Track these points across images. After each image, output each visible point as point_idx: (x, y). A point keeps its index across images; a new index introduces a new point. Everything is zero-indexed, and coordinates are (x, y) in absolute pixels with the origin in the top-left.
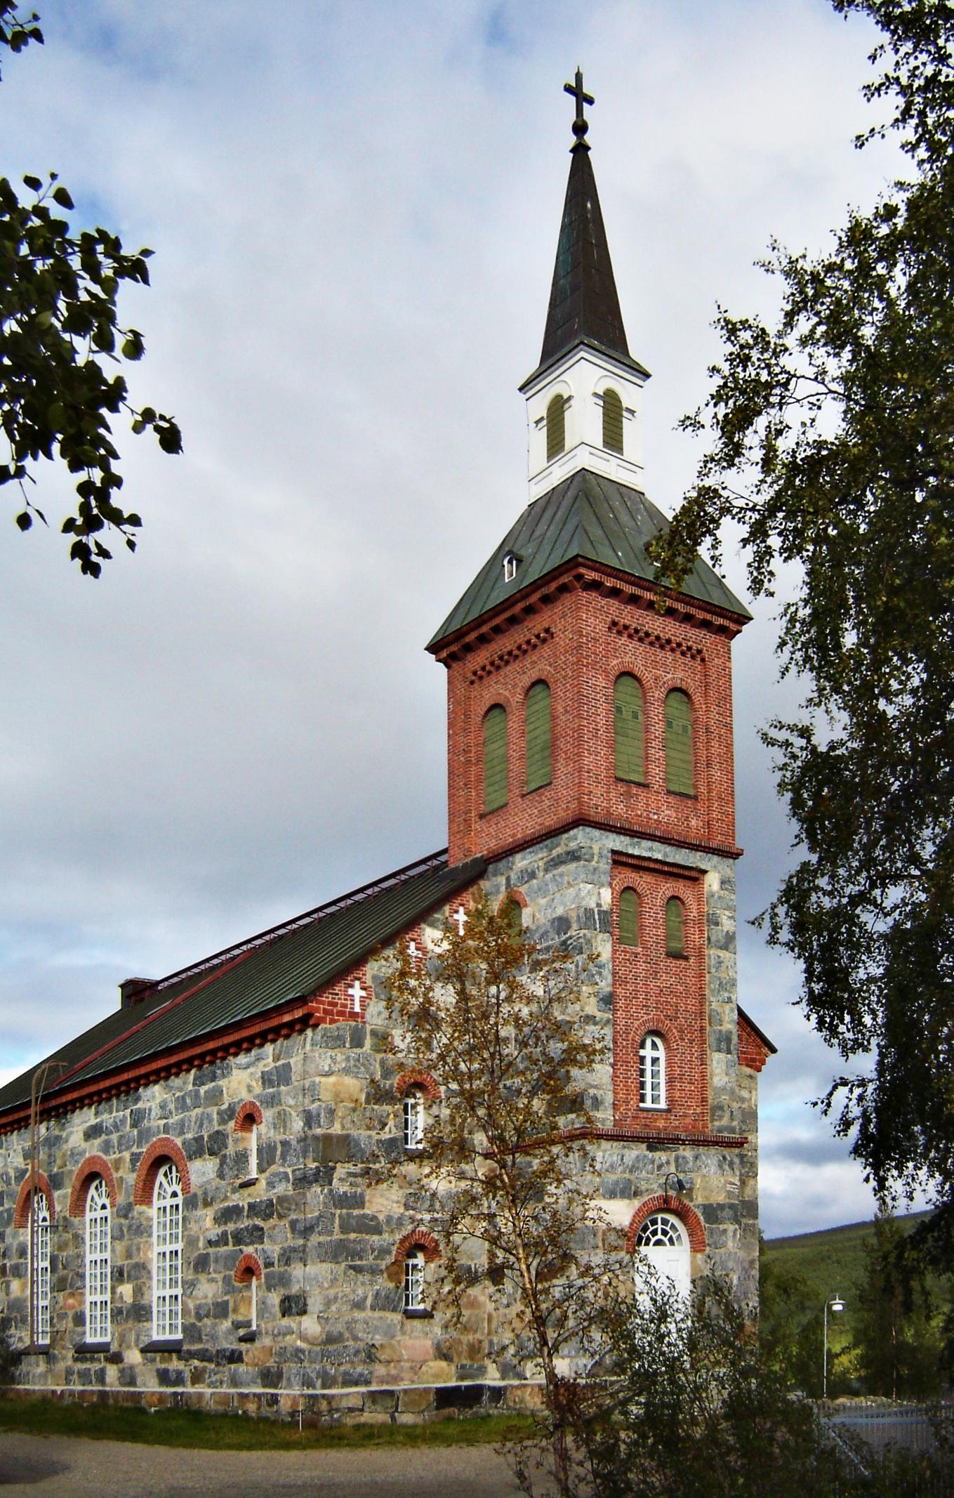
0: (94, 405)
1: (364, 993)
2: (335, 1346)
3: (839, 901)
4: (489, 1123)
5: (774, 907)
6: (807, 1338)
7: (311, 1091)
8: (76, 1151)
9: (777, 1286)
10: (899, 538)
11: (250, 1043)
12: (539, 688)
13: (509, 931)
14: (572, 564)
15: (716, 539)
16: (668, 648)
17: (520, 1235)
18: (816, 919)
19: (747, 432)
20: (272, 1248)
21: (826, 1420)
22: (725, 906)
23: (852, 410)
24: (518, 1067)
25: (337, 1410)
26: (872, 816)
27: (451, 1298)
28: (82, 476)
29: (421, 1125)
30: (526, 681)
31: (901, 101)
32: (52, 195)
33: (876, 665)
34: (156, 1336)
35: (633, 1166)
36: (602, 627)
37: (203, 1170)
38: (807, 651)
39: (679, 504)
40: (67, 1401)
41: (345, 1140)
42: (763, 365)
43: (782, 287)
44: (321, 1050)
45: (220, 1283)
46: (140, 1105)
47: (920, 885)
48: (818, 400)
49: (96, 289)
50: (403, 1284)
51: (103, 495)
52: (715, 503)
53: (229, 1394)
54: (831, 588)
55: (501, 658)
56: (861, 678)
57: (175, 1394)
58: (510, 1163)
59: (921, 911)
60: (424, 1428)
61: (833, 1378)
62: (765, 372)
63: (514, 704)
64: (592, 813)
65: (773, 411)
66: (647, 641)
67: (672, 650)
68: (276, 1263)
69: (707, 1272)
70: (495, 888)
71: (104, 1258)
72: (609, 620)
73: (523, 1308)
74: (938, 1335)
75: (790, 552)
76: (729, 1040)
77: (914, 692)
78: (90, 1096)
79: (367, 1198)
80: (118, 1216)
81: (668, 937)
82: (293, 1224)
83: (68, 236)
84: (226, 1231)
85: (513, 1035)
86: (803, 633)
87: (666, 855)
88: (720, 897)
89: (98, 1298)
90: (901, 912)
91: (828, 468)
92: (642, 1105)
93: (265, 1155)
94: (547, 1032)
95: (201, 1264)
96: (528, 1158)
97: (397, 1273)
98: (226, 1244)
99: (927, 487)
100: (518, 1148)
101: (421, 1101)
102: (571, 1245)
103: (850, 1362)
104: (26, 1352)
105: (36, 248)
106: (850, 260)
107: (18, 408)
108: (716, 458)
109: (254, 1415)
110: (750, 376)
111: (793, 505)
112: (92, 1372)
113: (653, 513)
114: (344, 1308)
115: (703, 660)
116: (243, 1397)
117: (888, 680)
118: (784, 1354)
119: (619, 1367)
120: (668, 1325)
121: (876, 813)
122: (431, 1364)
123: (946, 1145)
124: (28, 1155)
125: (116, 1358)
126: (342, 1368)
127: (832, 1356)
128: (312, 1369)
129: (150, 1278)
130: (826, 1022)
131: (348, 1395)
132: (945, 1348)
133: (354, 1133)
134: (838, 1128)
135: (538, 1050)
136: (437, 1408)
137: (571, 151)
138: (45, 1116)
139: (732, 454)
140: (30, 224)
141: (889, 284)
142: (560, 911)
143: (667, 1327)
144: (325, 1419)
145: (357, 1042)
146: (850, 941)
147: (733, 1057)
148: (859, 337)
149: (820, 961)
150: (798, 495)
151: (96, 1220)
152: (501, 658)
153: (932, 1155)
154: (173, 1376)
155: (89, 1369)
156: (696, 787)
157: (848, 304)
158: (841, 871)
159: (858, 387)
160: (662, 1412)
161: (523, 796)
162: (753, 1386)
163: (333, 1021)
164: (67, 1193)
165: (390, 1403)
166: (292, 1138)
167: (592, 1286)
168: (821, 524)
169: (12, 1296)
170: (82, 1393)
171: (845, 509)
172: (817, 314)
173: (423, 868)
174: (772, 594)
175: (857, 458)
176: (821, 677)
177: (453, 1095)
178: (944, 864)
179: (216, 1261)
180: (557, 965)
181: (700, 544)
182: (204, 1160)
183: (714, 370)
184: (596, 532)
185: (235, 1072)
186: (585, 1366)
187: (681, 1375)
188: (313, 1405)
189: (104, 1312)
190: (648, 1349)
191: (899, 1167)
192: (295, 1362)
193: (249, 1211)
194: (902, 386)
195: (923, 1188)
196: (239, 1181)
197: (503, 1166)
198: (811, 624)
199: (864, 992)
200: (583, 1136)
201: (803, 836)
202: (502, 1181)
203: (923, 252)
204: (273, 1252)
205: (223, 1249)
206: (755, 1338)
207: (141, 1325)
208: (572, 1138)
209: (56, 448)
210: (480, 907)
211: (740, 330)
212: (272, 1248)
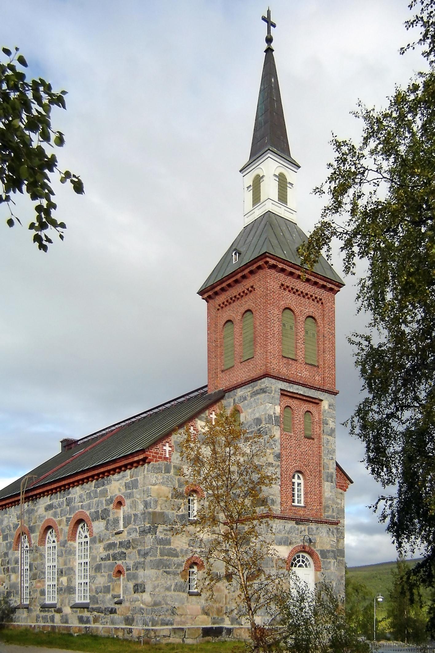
0: (42, 168)
1: (170, 449)
2: (158, 607)
3: (382, 416)
4: (226, 509)
5: (352, 418)
6: (366, 612)
7: (147, 492)
8: (41, 516)
9: (353, 589)
10: (413, 249)
11: (119, 469)
12: (248, 313)
13: (235, 424)
14: (263, 256)
15: (329, 247)
16: (306, 297)
17: (239, 560)
18: (371, 424)
19: (344, 196)
20: (130, 562)
21: (375, 650)
22: (330, 416)
23: (393, 187)
24: (238, 485)
25: (159, 636)
26: (398, 378)
27: (209, 587)
28: (37, 202)
29: (196, 509)
31: (423, 30)
32: (17, 59)
33: (401, 309)
34: (77, 601)
35: (289, 531)
36: (277, 286)
37: (99, 526)
38: (369, 301)
39: (312, 230)
40: (37, 630)
41: (162, 514)
42: (353, 164)
43: (362, 124)
44: (151, 474)
45: (106, 577)
46: (70, 496)
47: (419, 410)
48: (378, 181)
49: (41, 109)
50: (188, 580)
51: (47, 212)
52: (329, 230)
53: (110, 628)
54: (381, 272)
55: (231, 299)
56: (394, 315)
57: (86, 628)
58: (235, 528)
59: (419, 423)
60: (197, 645)
61: (378, 631)
62: (354, 167)
63: (237, 320)
64: (272, 372)
65: (356, 186)
66: (297, 293)
67: (308, 298)
68: (131, 569)
69: (322, 580)
70: (228, 403)
71: (54, 565)
72: (280, 283)
73: (241, 593)
74: (425, 615)
75: (363, 254)
76: (332, 477)
77: (418, 322)
78: (48, 491)
79: (172, 541)
80: (60, 546)
81: (305, 429)
82: (139, 551)
83: (25, 81)
84: (109, 554)
85: (237, 470)
86: (368, 293)
87: (304, 392)
88: (328, 412)
89: (51, 583)
90: (410, 422)
91: (381, 215)
92: (293, 504)
93: (126, 520)
94: (251, 469)
95: (98, 568)
96: (243, 526)
97: (185, 575)
98: (109, 560)
99: (427, 225)
100: (238, 521)
101: (196, 498)
102: (262, 565)
103: (386, 625)
104: (18, 608)
105: (10, 86)
106: (395, 112)
107: (5, 167)
108: (330, 208)
109: (121, 638)
110: (346, 169)
111: (365, 232)
112: (48, 617)
113: (301, 233)
114: (162, 590)
115: (322, 303)
116: (117, 629)
117: (406, 316)
118: (356, 619)
119: (283, 622)
120: (305, 603)
121: (399, 377)
122: (200, 616)
123: (429, 529)
124: (19, 517)
125: (59, 611)
126: (161, 617)
127: (378, 622)
128: (147, 617)
129: (75, 574)
130: (375, 471)
131: (163, 629)
132: (429, 621)
133: (166, 511)
134: (380, 519)
135: (248, 477)
136: (203, 637)
137: (265, 52)
138: (27, 500)
139: (337, 206)
140: (7, 73)
141: (414, 124)
142: (257, 415)
143: (304, 604)
144: (153, 640)
145: (168, 471)
146: (386, 435)
147: (334, 484)
148: (398, 151)
149: (373, 443)
150: (367, 228)
151: (50, 547)
152: (231, 299)
153: (423, 533)
154: (85, 619)
155: (47, 616)
156: (318, 362)
157: (393, 134)
158: (383, 403)
159: (397, 175)
160: (302, 643)
161: (241, 362)
162: (343, 633)
163: (156, 461)
164: (37, 535)
165: (182, 634)
166: (138, 513)
167: (271, 584)
168: (377, 242)
169: (12, 582)
170: (44, 626)
171: (389, 234)
172: (379, 139)
173: (196, 393)
174: (354, 274)
175: (395, 210)
176: (376, 313)
177: (209, 495)
178: (430, 401)
179: (105, 567)
180: (256, 439)
181: (322, 249)
183: (330, 165)
184: (274, 241)
185: (113, 482)
186: (268, 620)
187: (310, 626)
188: (148, 634)
189: (54, 590)
190: (296, 614)
191: (408, 538)
192: (140, 614)
193: (119, 545)
194: (418, 175)
195: (418, 548)
196: (115, 531)
197: (232, 529)
198: (372, 288)
199: (393, 458)
200: (267, 517)
201: (366, 386)
202: (232, 535)
203: (430, 109)
204: (130, 564)
205: (108, 562)
206: (343, 611)
207: (71, 595)
208: (262, 517)
209: (24, 188)
210: (222, 412)
211: (342, 146)
212: (130, 562)
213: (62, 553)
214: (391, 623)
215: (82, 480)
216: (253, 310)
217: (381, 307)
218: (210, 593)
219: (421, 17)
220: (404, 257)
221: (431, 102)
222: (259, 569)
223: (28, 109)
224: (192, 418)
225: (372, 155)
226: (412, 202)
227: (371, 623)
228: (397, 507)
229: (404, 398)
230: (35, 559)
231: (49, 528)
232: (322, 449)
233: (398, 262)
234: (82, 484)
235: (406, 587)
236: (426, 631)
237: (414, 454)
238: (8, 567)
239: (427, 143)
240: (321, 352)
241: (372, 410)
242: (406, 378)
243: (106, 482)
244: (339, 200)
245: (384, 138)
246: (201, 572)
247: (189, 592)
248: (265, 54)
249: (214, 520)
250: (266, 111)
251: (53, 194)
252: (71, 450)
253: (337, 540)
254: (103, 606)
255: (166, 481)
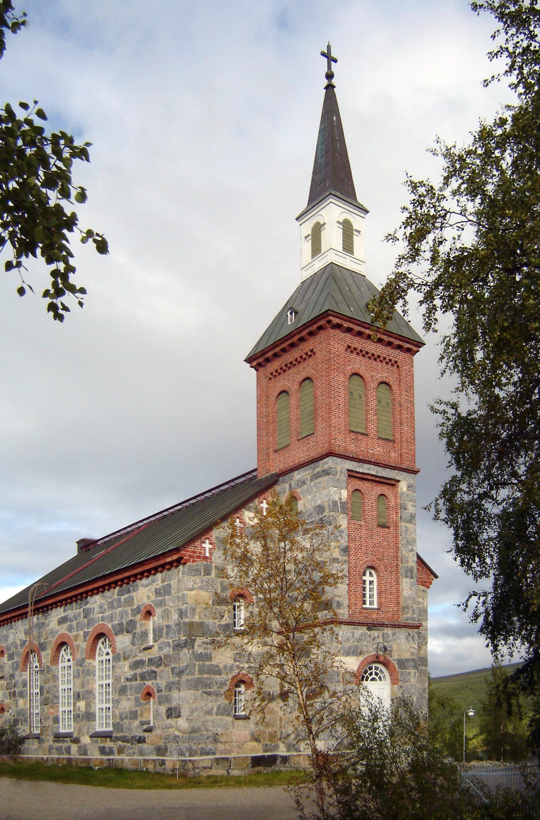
1: (211, 546)
2: (196, 734)
4: (280, 615)
6: (454, 730)
7: (182, 599)
9: (438, 703)
10: (506, 300)
11: (149, 573)
12: (307, 382)
14: (325, 315)
15: (405, 301)
16: (378, 360)
17: (297, 675)
19: (422, 243)
20: (162, 682)
21: (465, 773)
23: (481, 230)
24: (296, 586)
25: (197, 768)
27: (259, 709)
28: (53, 267)
29: (243, 616)
30: (301, 378)
31: (509, 61)
32: (35, 112)
33: (494, 369)
34: (98, 729)
35: (359, 639)
36: (342, 349)
38: (455, 362)
39: (385, 282)
40: (50, 763)
42: (431, 206)
43: (442, 163)
44: (188, 577)
45: (133, 701)
46: (88, 606)
47: (517, 488)
48: (462, 225)
50: (233, 701)
51: (65, 277)
52: (405, 281)
53: (138, 759)
54: (469, 328)
55: (286, 366)
56: (486, 377)
57: (109, 760)
58: (291, 637)
59: (518, 502)
60: (245, 777)
62: (433, 209)
63: (293, 391)
64: (337, 450)
65: (437, 231)
66: (367, 356)
67: (381, 361)
68: (164, 690)
69: (399, 695)
72: (346, 345)
73: (299, 714)
74: (526, 729)
75: (446, 308)
76: (412, 571)
77: (514, 384)
79: (213, 656)
80: (77, 665)
81: (378, 516)
82: (173, 670)
83: (44, 135)
86: (453, 352)
87: (377, 472)
88: (407, 495)
89: (66, 709)
90: (507, 503)
91: (467, 262)
92: (364, 606)
93: (157, 633)
95: (122, 691)
96: (302, 634)
97: (230, 696)
98: (136, 680)
99: (523, 273)
100: (295, 629)
101: (243, 604)
102: (325, 680)
103: (478, 742)
104: (27, 738)
105: (27, 142)
106: (480, 148)
107: (17, 229)
108: (405, 257)
109: (152, 770)
111: (448, 282)
112: (63, 748)
113: (370, 286)
115: (398, 367)
116: (146, 761)
117: (500, 378)
118: (441, 738)
122: (249, 743)
123: (531, 627)
125: (76, 741)
126: (200, 746)
127: (468, 740)
128: (184, 746)
129: (95, 698)
132: (530, 735)
133: (206, 621)
134: (472, 618)
135: (307, 576)
136: (252, 767)
137: (325, 88)
138: (36, 612)
140: (23, 129)
141: (502, 161)
142: (319, 502)
143: (377, 724)
144: (191, 773)
145: (208, 572)
146: (479, 518)
149: (462, 529)
150: (451, 277)
151: (65, 667)
152: (286, 366)
153: (523, 632)
154: (108, 750)
155: (62, 747)
156: (394, 435)
157: (479, 173)
159: (485, 218)
160: (375, 769)
161: (299, 440)
162: (425, 756)
163: (194, 561)
165: (226, 764)
166: (172, 623)
169: (19, 708)
170: (58, 759)
172: (462, 178)
174: (436, 331)
175: (484, 257)
176: (463, 376)
177: (260, 600)
178: (531, 477)
179: (131, 689)
180: (317, 531)
181: (396, 304)
182: (124, 635)
183: (404, 208)
184: (339, 297)
185: (140, 588)
186: (333, 745)
187: (385, 749)
188: (184, 765)
191: (505, 639)
193: (148, 662)
194: (509, 217)
195: (518, 650)
196: (143, 647)
197: (288, 639)
198: (458, 347)
199: (486, 546)
200: (332, 622)
201: (453, 462)
202: (287, 647)
203: (521, 144)
204: (162, 684)
205: (134, 683)
206: (426, 730)
207: (90, 723)
208: (325, 623)
209: (39, 251)
210: (275, 500)
212: (162, 682)
213: (79, 673)
214: (484, 740)
215: (103, 587)
216: (314, 378)
217: (469, 369)
218: (260, 715)
219: (506, 47)
220: (496, 309)
221: (521, 137)
222: (322, 686)
223: (46, 165)
224: (238, 509)
225: (454, 196)
226: (504, 248)
227: (460, 741)
228: (492, 604)
229: (499, 475)
230: (46, 681)
231: (63, 644)
232: (400, 538)
233: (489, 316)
234: (103, 592)
235: (503, 697)
236: (526, 747)
237: (512, 539)
238: (15, 691)
239: (519, 182)
240: (397, 424)
241: (460, 490)
242: (502, 450)
243: (131, 588)
244: (416, 247)
245: (468, 177)
246: (249, 691)
247: (235, 716)
248: (325, 90)
249: (265, 629)
250: (327, 151)
251: (72, 256)
252: (89, 553)
253: (418, 646)
254: (129, 735)
255: (206, 585)
